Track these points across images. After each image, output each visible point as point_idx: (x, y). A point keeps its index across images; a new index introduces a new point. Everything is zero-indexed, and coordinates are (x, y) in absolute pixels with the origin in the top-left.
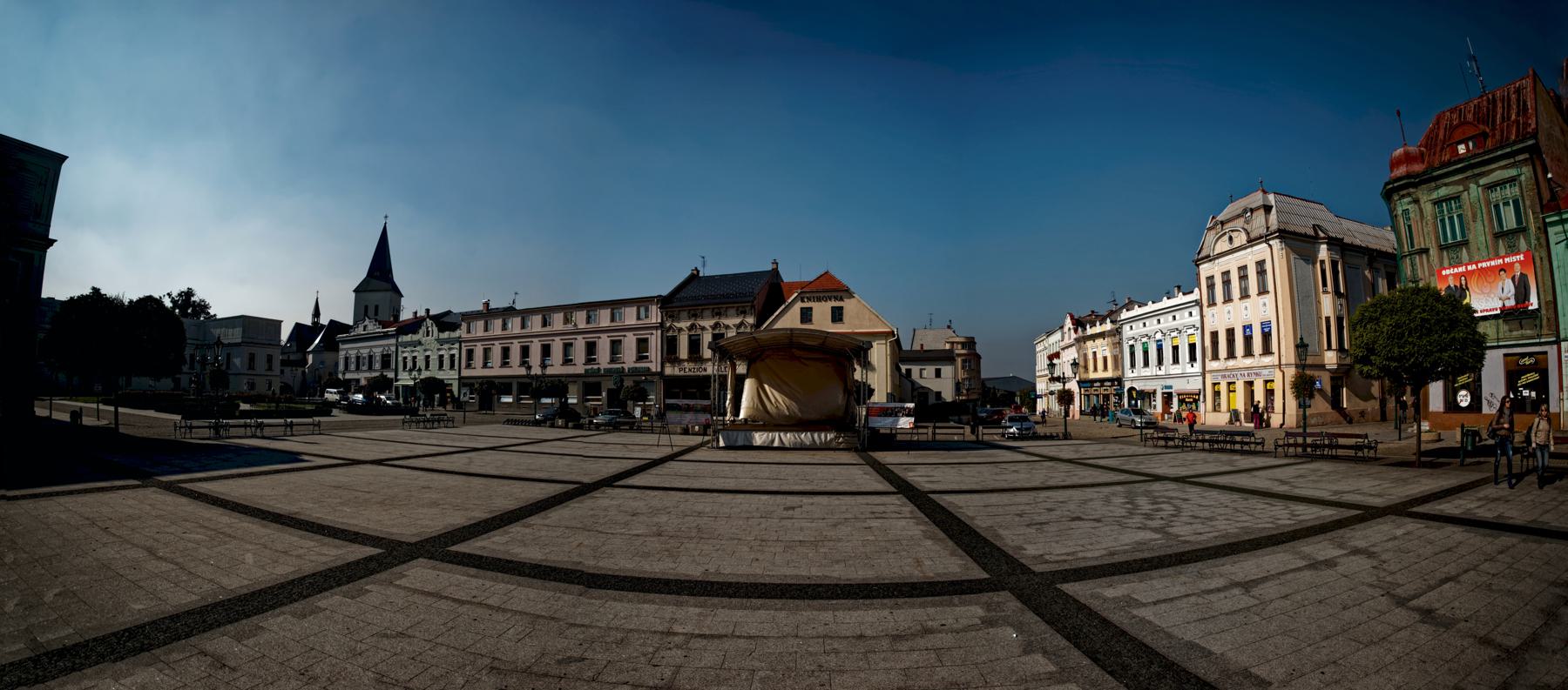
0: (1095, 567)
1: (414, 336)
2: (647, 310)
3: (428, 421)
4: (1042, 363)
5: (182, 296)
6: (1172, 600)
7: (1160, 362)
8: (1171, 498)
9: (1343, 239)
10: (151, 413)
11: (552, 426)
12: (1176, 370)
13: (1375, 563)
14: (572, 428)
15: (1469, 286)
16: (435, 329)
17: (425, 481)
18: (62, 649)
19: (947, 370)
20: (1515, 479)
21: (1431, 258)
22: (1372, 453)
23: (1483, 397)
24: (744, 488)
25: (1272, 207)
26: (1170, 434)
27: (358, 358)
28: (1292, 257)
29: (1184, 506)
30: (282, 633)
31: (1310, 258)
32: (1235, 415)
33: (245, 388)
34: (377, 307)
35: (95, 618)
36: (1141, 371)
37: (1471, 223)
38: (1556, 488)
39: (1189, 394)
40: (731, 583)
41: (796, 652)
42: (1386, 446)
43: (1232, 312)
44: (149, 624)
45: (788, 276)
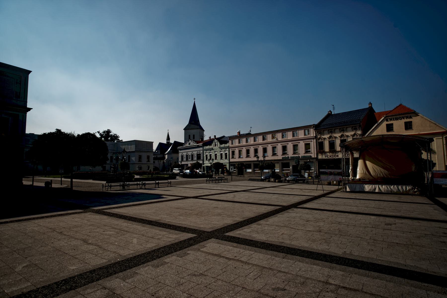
1: (210, 146)
2: (308, 131)
3: (217, 180)
5: (105, 133)
10: (91, 181)
11: (269, 181)
16: (219, 143)
17: (216, 205)
18: (20, 295)
27: (187, 156)
30: (146, 275)
33: (137, 169)
34: (194, 136)
35: (46, 276)
44: (77, 276)
45: (377, 109)
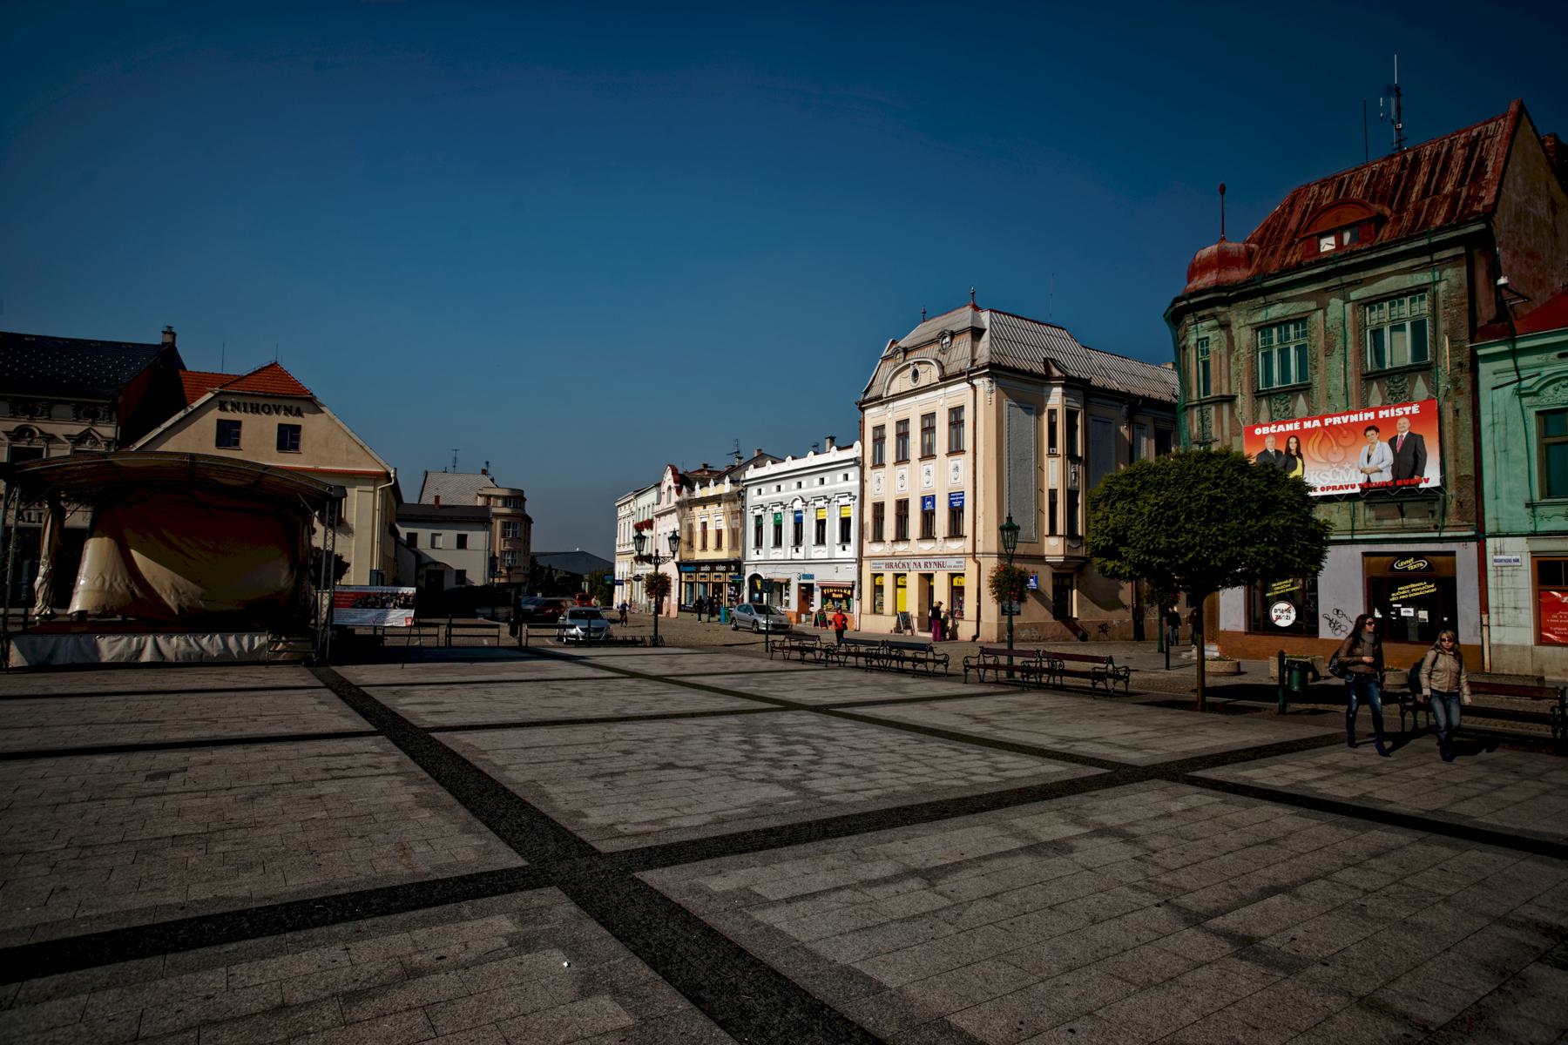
0: (694, 843)
4: (625, 535)
6: (814, 895)
7: (798, 540)
8: (809, 736)
9: (1090, 380)
12: (820, 553)
13: (1138, 853)
15: (1303, 451)
19: (477, 538)
20: (1390, 741)
21: (1237, 412)
22: (1120, 685)
23: (1321, 613)
25: (984, 330)
26: (808, 643)
28: (1005, 404)
29: (829, 749)
31: (1034, 406)
32: (904, 620)
36: (769, 552)
37: (1322, 358)
38: (1480, 763)
42: (1146, 676)
43: (932, 473)
45: (194, 359)
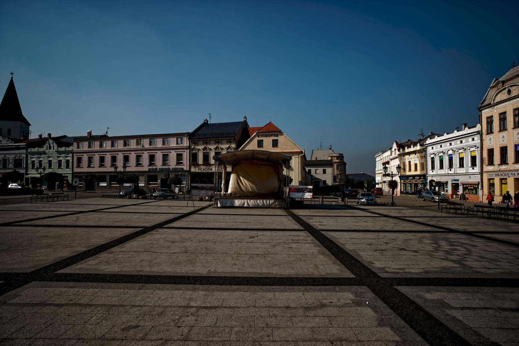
2: (182, 140)
4: (379, 167)
7: (451, 166)
8: (463, 243)
11: (130, 198)
14: (141, 199)
19: (329, 170)
24: (230, 227)
29: (473, 249)
36: (438, 171)
39: (471, 185)
40: (222, 277)
41: (254, 316)
43: (506, 137)
45: (252, 124)
